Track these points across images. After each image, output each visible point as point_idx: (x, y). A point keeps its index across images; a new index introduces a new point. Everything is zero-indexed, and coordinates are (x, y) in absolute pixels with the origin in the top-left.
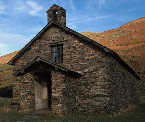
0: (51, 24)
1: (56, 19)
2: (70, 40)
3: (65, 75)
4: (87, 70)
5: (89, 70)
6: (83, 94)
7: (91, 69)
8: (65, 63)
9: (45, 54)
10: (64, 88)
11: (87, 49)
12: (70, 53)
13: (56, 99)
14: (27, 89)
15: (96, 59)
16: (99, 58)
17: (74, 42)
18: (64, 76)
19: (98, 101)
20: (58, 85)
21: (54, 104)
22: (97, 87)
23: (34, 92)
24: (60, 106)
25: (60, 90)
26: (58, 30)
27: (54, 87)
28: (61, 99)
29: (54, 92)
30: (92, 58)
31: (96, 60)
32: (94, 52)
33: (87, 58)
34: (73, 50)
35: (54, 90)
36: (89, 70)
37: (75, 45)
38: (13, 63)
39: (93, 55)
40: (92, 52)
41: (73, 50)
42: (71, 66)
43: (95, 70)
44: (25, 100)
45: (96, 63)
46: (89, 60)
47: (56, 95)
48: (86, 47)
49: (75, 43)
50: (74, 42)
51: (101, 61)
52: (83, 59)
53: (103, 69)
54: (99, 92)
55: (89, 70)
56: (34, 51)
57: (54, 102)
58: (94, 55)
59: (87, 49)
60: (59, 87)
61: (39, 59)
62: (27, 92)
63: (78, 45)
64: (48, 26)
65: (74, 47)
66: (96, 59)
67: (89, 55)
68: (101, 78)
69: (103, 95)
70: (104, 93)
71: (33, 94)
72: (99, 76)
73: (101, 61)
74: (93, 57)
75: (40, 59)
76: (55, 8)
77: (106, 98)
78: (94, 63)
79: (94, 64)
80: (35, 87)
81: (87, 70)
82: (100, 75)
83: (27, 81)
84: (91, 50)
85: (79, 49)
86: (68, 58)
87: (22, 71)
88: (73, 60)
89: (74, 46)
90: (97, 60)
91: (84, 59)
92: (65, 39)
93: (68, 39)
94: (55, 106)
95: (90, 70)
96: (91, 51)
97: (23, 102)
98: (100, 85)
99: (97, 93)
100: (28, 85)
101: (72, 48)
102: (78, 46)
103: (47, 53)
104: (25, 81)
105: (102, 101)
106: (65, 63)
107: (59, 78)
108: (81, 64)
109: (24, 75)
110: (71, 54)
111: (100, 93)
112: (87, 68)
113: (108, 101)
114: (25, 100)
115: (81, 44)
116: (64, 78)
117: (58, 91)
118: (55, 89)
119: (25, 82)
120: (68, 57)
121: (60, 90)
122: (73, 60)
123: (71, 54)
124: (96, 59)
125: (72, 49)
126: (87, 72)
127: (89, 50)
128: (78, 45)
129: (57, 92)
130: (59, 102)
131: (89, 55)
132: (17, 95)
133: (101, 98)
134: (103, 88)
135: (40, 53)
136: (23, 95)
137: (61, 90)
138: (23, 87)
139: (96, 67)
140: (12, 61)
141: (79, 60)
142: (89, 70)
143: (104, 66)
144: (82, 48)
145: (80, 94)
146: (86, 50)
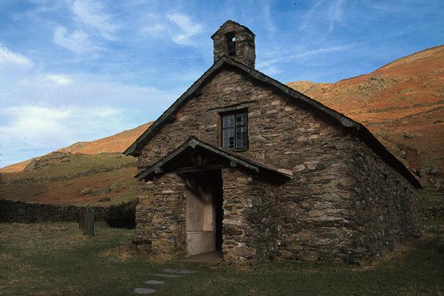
0: (221, 63)
1: (233, 54)
2: (265, 100)
3: (253, 178)
4: (301, 168)
6: (294, 220)
7: (311, 164)
9: (207, 131)
10: (251, 206)
11: (303, 120)
12: (265, 129)
13: (232, 232)
14: (168, 209)
16: (328, 139)
17: (274, 103)
18: (250, 179)
20: (237, 200)
21: (228, 243)
25: (241, 210)
26: (238, 77)
28: (243, 231)
29: (228, 217)
30: (313, 141)
31: (322, 145)
32: (317, 125)
33: (302, 139)
34: (272, 121)
36: (306, 166)
37: (275, 111)
39: (316, 133)
40: (313, 126)
41: (272, 121)
43: (320, 167)
44: (164, 234)
45: (322, 151)
46: (305, 144)
47: (232, 222)
48: (300, 116)
49: (274, 107)
50: (274, 103)
51: (334, 148)
54: (329, 215)
56: (185, 124)
57: (228, 238)
58: (319, 134)
59: (303, 120)
60: (239, 204)
61: (193, 144)
62: (168, 215)
63: (282, 110)
64: (215, 67)
65: (272, 116)
66: (323, 143)
67: (306, 134)
68: (333, 184)
69: (337, 222)
70: (339, 218)
72: (328, 181)
74: (315, 137)
75: (198, 143)
76: (230, 29)
78: (318, 150)
79: (318, 154)
81: (301, 168)
82: (332, 177)
83: (167, 192)
87: (157, 170)
88: (270, 144)
89: (274, 114)
90: (325, 144)
91: (296, 142)
93: (260, 96)
94: (230, 247)
95: (309, 167)
96: (311, 124)
97: (159, 237)
98: (331, 201)
99: (324, 218)
103: (212, 130)
104: (163, 192)
105: (334, 236)
107: (240, 185)
108: (289, 153)
109: (162, 178)
111: (332, 219)
112: (302, 163)
113: (349, 235)
114: (164, 234)
115: (288, 109)
116: (250, 183)
117: (236, 214)
118: (230, 208)
119: (164, 194)
120: (260, 137)
121: (241, 210)
122: (270, 144)
126: (302, 172)
128: (282, 110)
129: (235, 216)
130: (240, 239)
131: (306, 134)
133: (334, 230)
134: (337, 207)
135: (197, 129)
138: (160, 206)
139: (322, 160)
142: (306, 166)
143: (339, 158)
145: (286, 220)
146: (300, 121)
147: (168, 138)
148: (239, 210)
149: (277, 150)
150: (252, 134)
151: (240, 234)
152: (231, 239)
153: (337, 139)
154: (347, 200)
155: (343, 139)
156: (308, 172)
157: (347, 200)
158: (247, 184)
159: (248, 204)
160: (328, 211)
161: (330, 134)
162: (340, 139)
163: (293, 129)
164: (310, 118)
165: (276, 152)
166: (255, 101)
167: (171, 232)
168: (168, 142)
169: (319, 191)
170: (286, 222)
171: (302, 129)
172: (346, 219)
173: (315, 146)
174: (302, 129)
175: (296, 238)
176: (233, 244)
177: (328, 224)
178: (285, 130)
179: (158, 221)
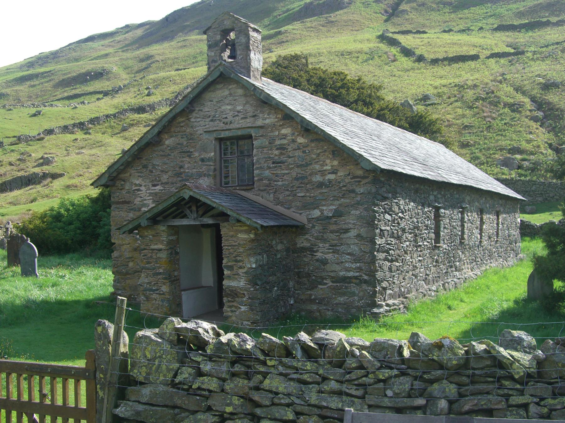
0: (218, 74)
2: (273, 126)
4: (316, 213)
5: (322, 213)
6: (308, 275)
7: (328, 210)
8: (259, 190)
9: (203, 160)
10: (254, 266)
12: (273, 163)
13: (235, 294)
14: (159, 267)
15: (339, 182)
16: (347, 181)
17: (284, 131)
19: (344, 294)
20: (239, 258)
21: (230, 307)
22: (342, 257)
23: (176, 273)
24: (245, 312)
25: (244, 271)
26: (240, 91)
27: (229, 264)
28: (245, 293)
29: (229, 277)
30: (330, 181)
31: (340, 188)
32: (335, 163)
33: (318, 178)
34: (281, 154)
35: (229, 272)
36: (322, 211)
38: (110, 183)
39: (333, 173)
41: (281, 154)
42: (276, 199)
43: (338, 214)
44: (154, 296)
46: (321, 185)
47: (233, 284)
49: (285, 136)
50: (284, 131)
51: (353, 191)
52: (306, 181)
53: (358, 212)
54: (348, 270)
55: (322, 213)
56: (173, 149)
57: (229, 301)
58: (336, 173)
60: (241, 264)
61: (187, 195)
62: (160, 274)
63: (294, 141)
64: (210, 79)
65: (282, 148)
67: (323, 173)
68: (353, 233)
69: (356, 278)
70: (357, 274)
71: (174, 281)
72: (347, 231)
73: (353, 191)
74: (332, 177)
75: (191, 194)
77: (364, 286)
78: (335, 193)
79: (336, 198)
80: (178, 260)
81: (316, 213)
82: (351, 226)
83: (156, 247)
84: (328, 158)
85: (297, 154)
86: (267, 178)
88: (280, 183)
89: (284, 144)
90: (345, 186)
91: (310, 182)
92: (259, 123)
93: (267, 121)
94: (232, 311)
95: (325, 213)
96: (328, 161)
97: (148, 299)
98: (349, 254)
100: (159, 258)
101: (277, 149)
102: (292, 145)
103: (209, 159)
104: (153, 247)
105: (354, 294)
106: (259, 190)
108: (303, 195)
110: (276, 167)
111: (351, 274)
113: (369, 293)
114: (154, 296)
115: (301, 140)
116: (252, 241)
117: (238, 274)
118: (230, 268)
119: (152, 250)
120: (267, 173)
122: (280, 183)
123: (276, 167)
124: (339, 182)
125: (277, 152)
126: (318, 219)
127: (322, 158)
129: (237, 276)
132: (127, 273)
133: (354, 288)
134: (356, 261)
135: (189, 156)
136: (148, 283)
137: (245, 273)
138: (148, 263)
139: (340, 205)
140: (107, 175)
141: (297, 183)
142: (322, 211)
143: (358, 203)
144: (304, 152)
145: (298, 274)
146: (314, 156)
147: (150, 167)
148: (240, 270)
149: (288, 190)
150: (260, 95)
151: (242, 297)
152: (233, 302)
153: (356, 182)
154: (367, 253)
155: (364, 182)
156: (324, 220)
157: (367, 253)
158: (249, 242)
159: (251, 263)
160: (347, 265)
161: (349, 175)
162: (360, 181)
163: (307, 165)
164: (327, 154)
165: (287, 193)
166: (261, 127)
167: (163, 294)
168: (152, 172)
169: (335, 242)
170: (299, 277)
171: (317, 167)
172: (366, 275)
173: (333, 189)
174: (317, 167)
175: (311, 295)
176: (236, 307)
177: (345, 280)
178: (298, 167)
179: (146, 281)
